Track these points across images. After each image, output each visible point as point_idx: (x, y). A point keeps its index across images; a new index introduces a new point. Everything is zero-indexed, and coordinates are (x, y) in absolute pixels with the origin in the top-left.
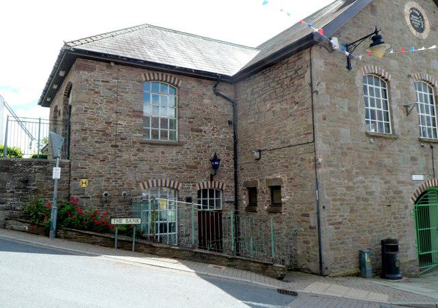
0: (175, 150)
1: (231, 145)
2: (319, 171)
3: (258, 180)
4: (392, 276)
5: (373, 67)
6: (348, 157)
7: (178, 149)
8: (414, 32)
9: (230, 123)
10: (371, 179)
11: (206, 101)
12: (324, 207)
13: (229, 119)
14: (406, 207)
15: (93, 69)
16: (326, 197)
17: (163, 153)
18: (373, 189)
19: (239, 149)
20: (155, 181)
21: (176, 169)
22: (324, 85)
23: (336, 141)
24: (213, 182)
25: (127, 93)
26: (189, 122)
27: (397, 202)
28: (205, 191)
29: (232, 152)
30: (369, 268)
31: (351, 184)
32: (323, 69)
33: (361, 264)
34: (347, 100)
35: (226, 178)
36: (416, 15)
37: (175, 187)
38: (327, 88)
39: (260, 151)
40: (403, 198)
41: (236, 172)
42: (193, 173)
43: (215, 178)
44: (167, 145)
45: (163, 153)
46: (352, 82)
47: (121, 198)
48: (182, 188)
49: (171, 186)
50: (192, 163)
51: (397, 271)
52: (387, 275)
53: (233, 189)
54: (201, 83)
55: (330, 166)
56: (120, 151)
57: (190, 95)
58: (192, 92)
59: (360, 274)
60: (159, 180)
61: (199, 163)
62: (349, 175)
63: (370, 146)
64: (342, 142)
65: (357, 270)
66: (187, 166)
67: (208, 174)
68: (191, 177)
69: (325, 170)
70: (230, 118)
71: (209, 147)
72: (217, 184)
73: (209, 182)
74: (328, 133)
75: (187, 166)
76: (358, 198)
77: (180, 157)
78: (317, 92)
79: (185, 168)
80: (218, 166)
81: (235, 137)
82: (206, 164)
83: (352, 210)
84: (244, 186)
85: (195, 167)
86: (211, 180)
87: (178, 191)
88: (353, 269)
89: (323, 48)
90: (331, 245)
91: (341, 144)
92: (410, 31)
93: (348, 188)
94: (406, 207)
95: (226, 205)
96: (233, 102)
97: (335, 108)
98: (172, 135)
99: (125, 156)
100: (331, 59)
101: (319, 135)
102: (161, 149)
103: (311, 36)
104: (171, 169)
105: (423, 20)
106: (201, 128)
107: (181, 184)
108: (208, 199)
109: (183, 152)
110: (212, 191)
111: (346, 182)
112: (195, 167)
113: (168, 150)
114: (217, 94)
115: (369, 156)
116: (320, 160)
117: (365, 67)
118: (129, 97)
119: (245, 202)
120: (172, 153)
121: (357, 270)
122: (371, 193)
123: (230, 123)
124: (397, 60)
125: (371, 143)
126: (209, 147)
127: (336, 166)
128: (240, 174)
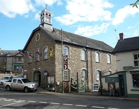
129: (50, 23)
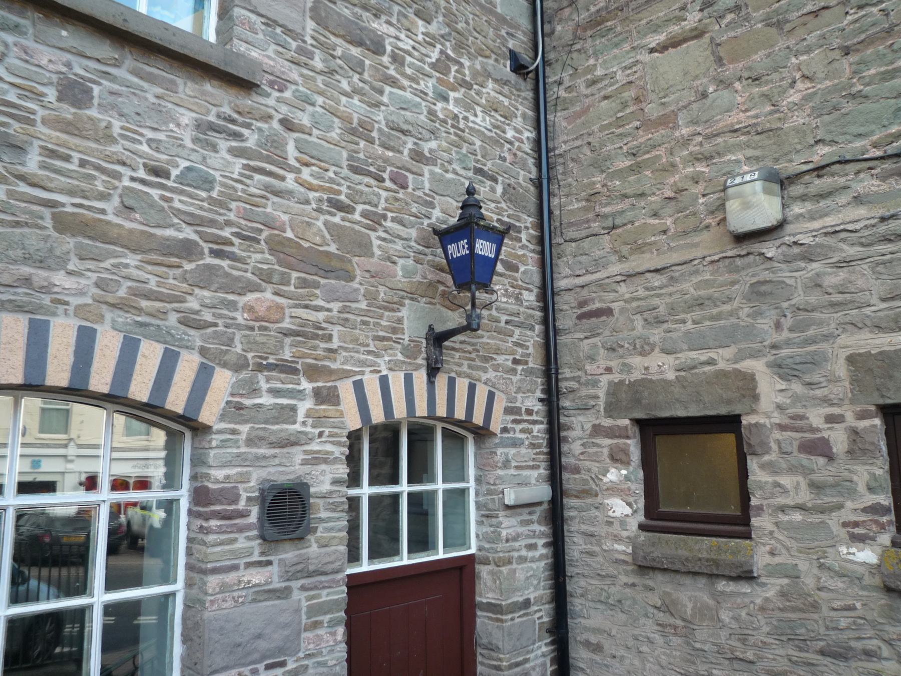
3: (757, 366)
7: (221, 101)
13: (511, 44)
15: (172, 88)
17: (74, 92)
19: (567, 204)
21: (187, 250)
24: (441, 381)
28: (385, 438)
35: (503, 360)
42: (323, 309)
43: (454, 356)
45: (74, 92)
48: (234, 411)
53: (539, 429)
61: (365, 248)
66: (277, 246)
67: (413, 321)
68: (305, 333)
70: (519, 43)
71: (417, 156)
73: (420, 377)
75: (277, 246)
79: (260, 258)
82: (400, 255)
84: (612, 409)
85: (331, 268)
87: (200, 430)
95: (509, 525)
104: (135, 244)
106: (379, 26)
107: (223, 381)
109: (252, 140)
110: (420, 435)
119: (619, 507)
123: (519, 68)
126: (417, 156)
128: (574, 340)
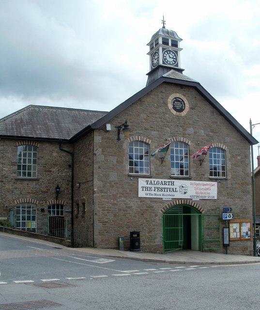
0: (34, 183)
1: (70, 179)
2: (94, 195)
4: (136, 250)
5: (137, 137)
6: (114, 188)
8: (174, 112)
9: (70, 166)
10: (129, 200)
11: (55, 154)
12: (96, 214)
14: (156, 215)
16: (98, 209)
17: (28, 184)
18: (132, 204)
20: (23, 200)
22: (100, 150)
23: (107, 179)
24: (58, 201)
25: (9, 153)
26: (44, 167)
27: (149, 212)
29: (70, 183)
30: (121, 245)
31: (115, 202)
32: (101, 142)
33: (118, 243)
34: (116, 157)
36: (179, 101)
37: (28, 202)
38: (103, 151)
39: (80, 183)
40: (154, 210)
41: (72, 195)
42: (45, 195)
44: (30, 180)
45: (28, 184)
46: (121, 147)
47: (5, 208)
49: (28, 202)
50: (45, 190)
51: (138, 247)
52: (132, 250)
54: (182, 88)
55: (102, 193)
56: (4, 184)
57: (45, 151)
58: (46, 150)
59: (118, 247)
60: (25, 199)
61: (49, 190)
62: (114, 197)
63: (130, 182)
64: (110, 180)
65: (117, 246)
68: (44, 198)
69: (98, 195)
71: (55, 180)
72: (60, 202)
74: (101, 175)
76: (120, 210)
77: (38, 186)
78: (95, 154)
79: (41, 192)
80: (56, 188)
81: (73, 174)
83: (115, 216)
85: (47, 192)
86: (57, 200)
88: (114, 245)
89: (101, 130)
90: (99, 233)
91: (110, 181)
92: (171, 112)
93: (113, 204)
94: (156, 215)
96: (71, 154)
97: (107, 161)
98: (29, 174)
99: (7, 187)
100: (107, 135)
101: (96, 176)
102: (26, 182)
103: (89, 127)
105: (184, 104)
108: (60, 210)
111: (112, 201)
112: (47, 192)
113: (30, 183)
114: (62, 150)
115: (130, 187)
116: (95, 190)
117: (131, 138)
118: (9, 155)
120: (33, 185)
121: (115, 246)
122: (130, 207)
123: (70, 166)
124: (158, 131)
125: (131, 180)
127: (106, 193)
129: (177, 65)
